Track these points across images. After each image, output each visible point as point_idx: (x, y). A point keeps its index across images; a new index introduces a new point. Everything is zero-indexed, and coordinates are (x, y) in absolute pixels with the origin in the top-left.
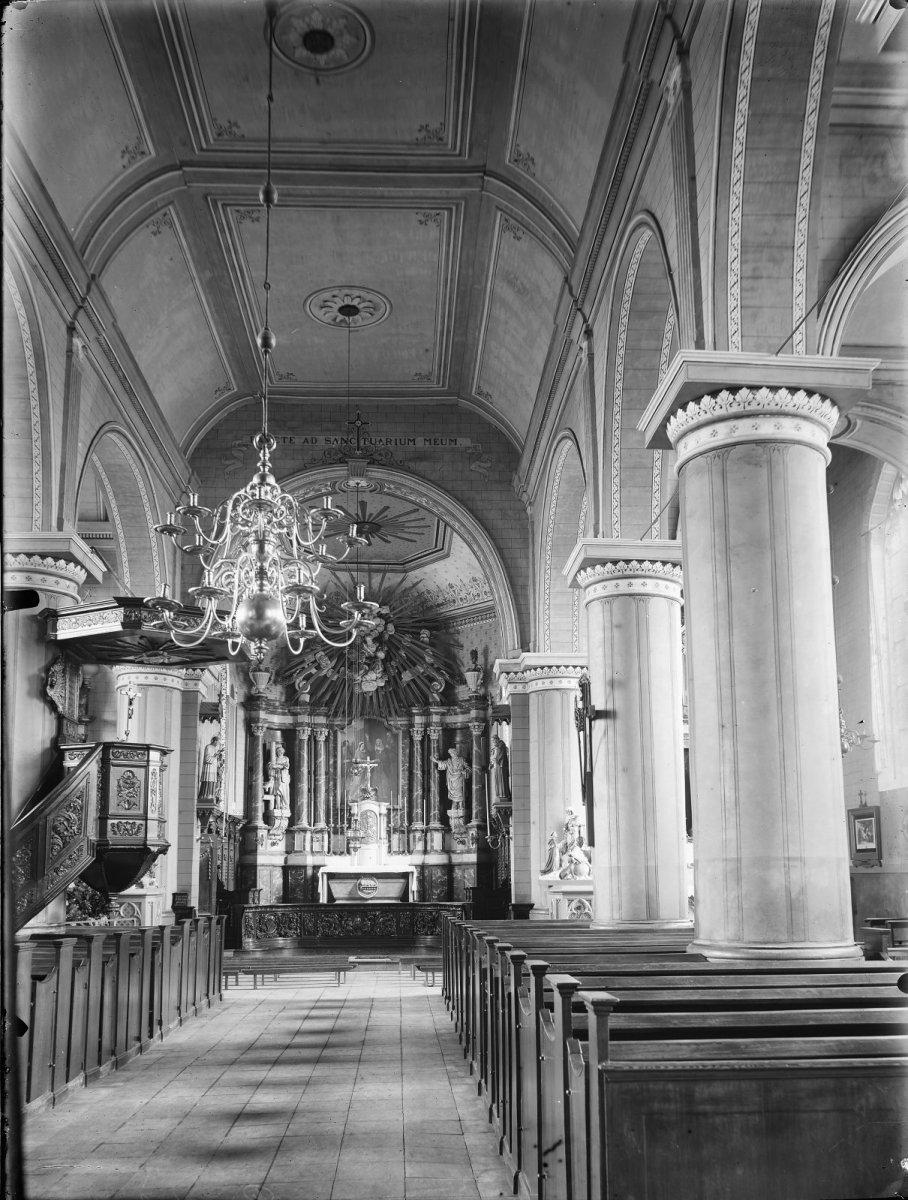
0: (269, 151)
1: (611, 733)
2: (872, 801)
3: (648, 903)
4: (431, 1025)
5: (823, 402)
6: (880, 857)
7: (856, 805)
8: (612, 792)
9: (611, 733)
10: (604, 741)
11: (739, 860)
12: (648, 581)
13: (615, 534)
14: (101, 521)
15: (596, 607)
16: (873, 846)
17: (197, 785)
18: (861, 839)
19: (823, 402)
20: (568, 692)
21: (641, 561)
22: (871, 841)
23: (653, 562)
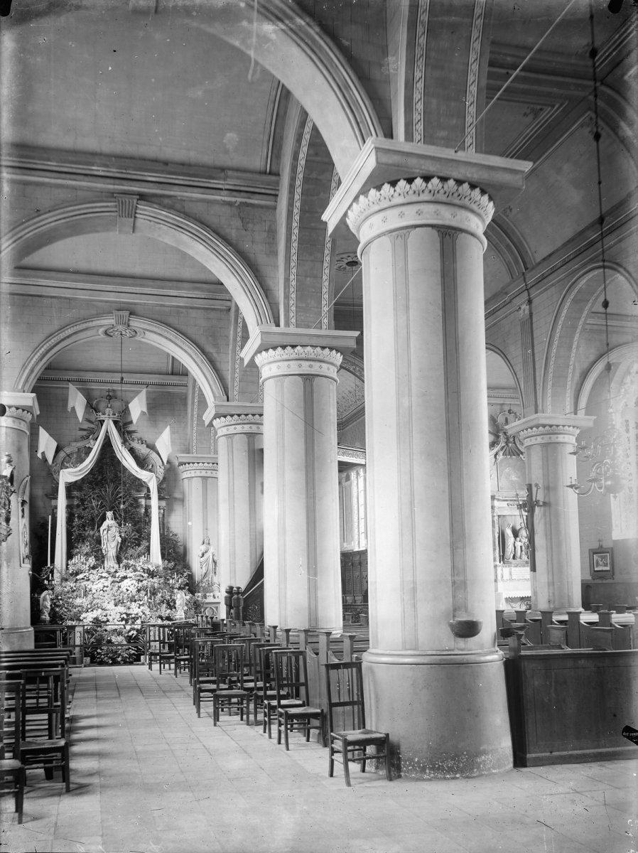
0: (607, 325)
1: (547, 514)
2: (607, 544)
3: (569, 600)
4: (223, 718)
5: (482, 195)
6: (613, 574)
7: (595, 546)
8: (549, 544)
9: (547, 514)
10: (543, 520)
11: (414, 582)
12: (566, 436)
13: (549, 411)
14: (168, 374)
15: (538, 449)
16: (608, 568)
17: (541, 556)
18: (598, 565)
19: (482, 195)
20: (17, 416)
21: (564, 426)
22: (606, 565)
23: (569, 426)
